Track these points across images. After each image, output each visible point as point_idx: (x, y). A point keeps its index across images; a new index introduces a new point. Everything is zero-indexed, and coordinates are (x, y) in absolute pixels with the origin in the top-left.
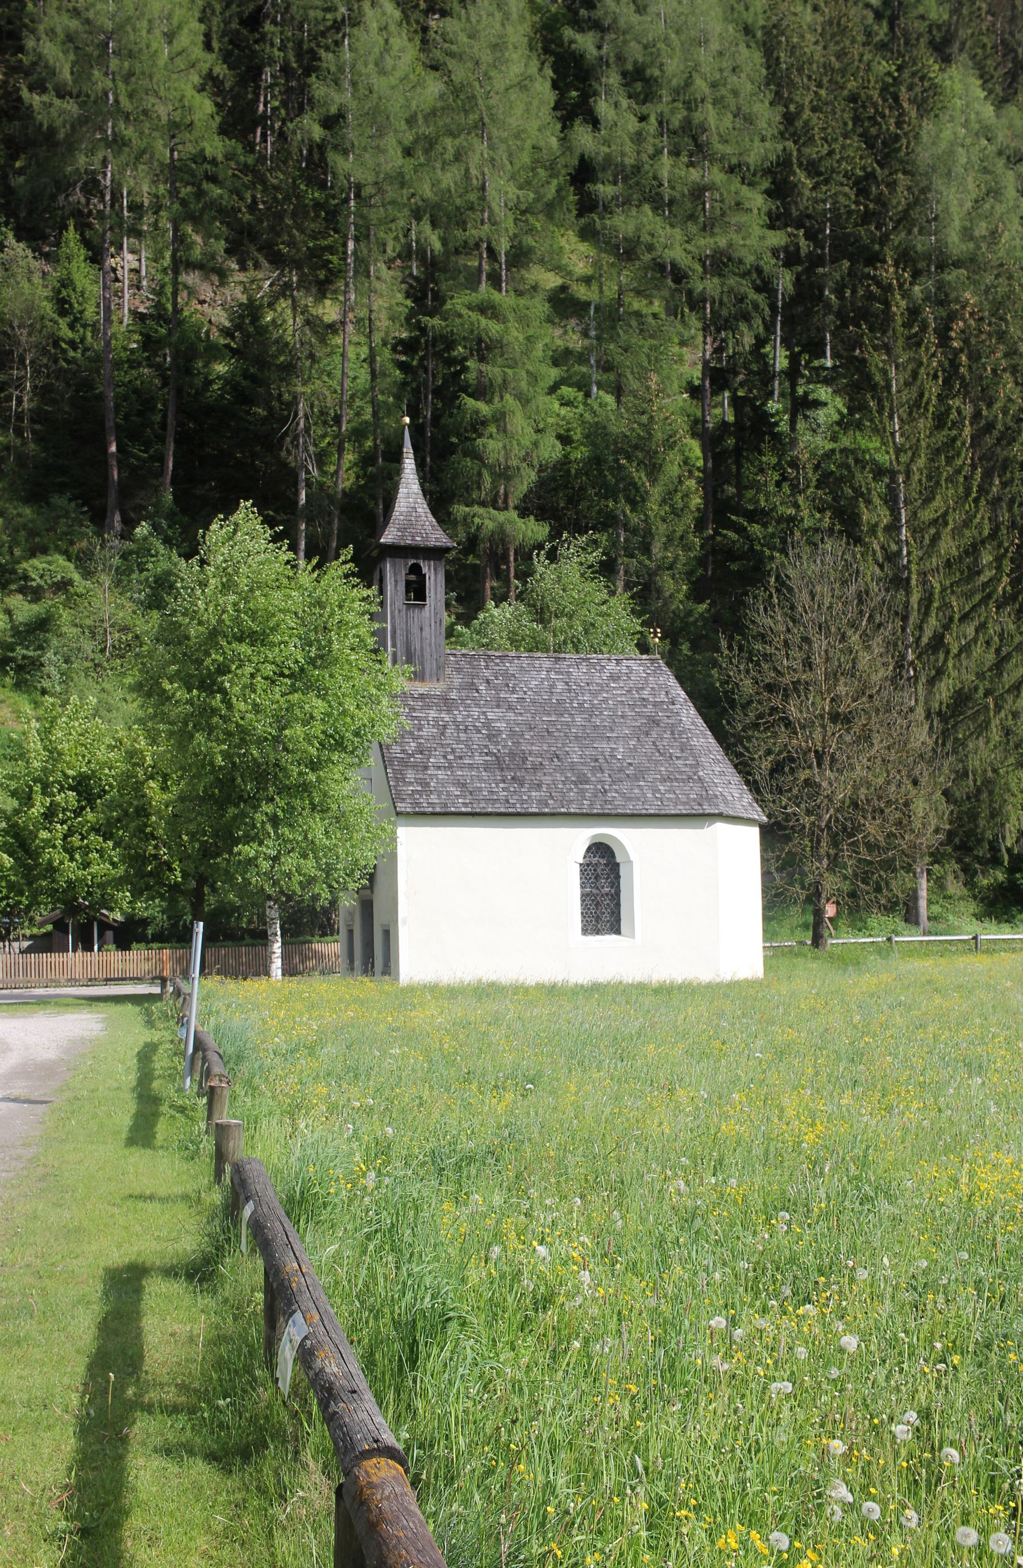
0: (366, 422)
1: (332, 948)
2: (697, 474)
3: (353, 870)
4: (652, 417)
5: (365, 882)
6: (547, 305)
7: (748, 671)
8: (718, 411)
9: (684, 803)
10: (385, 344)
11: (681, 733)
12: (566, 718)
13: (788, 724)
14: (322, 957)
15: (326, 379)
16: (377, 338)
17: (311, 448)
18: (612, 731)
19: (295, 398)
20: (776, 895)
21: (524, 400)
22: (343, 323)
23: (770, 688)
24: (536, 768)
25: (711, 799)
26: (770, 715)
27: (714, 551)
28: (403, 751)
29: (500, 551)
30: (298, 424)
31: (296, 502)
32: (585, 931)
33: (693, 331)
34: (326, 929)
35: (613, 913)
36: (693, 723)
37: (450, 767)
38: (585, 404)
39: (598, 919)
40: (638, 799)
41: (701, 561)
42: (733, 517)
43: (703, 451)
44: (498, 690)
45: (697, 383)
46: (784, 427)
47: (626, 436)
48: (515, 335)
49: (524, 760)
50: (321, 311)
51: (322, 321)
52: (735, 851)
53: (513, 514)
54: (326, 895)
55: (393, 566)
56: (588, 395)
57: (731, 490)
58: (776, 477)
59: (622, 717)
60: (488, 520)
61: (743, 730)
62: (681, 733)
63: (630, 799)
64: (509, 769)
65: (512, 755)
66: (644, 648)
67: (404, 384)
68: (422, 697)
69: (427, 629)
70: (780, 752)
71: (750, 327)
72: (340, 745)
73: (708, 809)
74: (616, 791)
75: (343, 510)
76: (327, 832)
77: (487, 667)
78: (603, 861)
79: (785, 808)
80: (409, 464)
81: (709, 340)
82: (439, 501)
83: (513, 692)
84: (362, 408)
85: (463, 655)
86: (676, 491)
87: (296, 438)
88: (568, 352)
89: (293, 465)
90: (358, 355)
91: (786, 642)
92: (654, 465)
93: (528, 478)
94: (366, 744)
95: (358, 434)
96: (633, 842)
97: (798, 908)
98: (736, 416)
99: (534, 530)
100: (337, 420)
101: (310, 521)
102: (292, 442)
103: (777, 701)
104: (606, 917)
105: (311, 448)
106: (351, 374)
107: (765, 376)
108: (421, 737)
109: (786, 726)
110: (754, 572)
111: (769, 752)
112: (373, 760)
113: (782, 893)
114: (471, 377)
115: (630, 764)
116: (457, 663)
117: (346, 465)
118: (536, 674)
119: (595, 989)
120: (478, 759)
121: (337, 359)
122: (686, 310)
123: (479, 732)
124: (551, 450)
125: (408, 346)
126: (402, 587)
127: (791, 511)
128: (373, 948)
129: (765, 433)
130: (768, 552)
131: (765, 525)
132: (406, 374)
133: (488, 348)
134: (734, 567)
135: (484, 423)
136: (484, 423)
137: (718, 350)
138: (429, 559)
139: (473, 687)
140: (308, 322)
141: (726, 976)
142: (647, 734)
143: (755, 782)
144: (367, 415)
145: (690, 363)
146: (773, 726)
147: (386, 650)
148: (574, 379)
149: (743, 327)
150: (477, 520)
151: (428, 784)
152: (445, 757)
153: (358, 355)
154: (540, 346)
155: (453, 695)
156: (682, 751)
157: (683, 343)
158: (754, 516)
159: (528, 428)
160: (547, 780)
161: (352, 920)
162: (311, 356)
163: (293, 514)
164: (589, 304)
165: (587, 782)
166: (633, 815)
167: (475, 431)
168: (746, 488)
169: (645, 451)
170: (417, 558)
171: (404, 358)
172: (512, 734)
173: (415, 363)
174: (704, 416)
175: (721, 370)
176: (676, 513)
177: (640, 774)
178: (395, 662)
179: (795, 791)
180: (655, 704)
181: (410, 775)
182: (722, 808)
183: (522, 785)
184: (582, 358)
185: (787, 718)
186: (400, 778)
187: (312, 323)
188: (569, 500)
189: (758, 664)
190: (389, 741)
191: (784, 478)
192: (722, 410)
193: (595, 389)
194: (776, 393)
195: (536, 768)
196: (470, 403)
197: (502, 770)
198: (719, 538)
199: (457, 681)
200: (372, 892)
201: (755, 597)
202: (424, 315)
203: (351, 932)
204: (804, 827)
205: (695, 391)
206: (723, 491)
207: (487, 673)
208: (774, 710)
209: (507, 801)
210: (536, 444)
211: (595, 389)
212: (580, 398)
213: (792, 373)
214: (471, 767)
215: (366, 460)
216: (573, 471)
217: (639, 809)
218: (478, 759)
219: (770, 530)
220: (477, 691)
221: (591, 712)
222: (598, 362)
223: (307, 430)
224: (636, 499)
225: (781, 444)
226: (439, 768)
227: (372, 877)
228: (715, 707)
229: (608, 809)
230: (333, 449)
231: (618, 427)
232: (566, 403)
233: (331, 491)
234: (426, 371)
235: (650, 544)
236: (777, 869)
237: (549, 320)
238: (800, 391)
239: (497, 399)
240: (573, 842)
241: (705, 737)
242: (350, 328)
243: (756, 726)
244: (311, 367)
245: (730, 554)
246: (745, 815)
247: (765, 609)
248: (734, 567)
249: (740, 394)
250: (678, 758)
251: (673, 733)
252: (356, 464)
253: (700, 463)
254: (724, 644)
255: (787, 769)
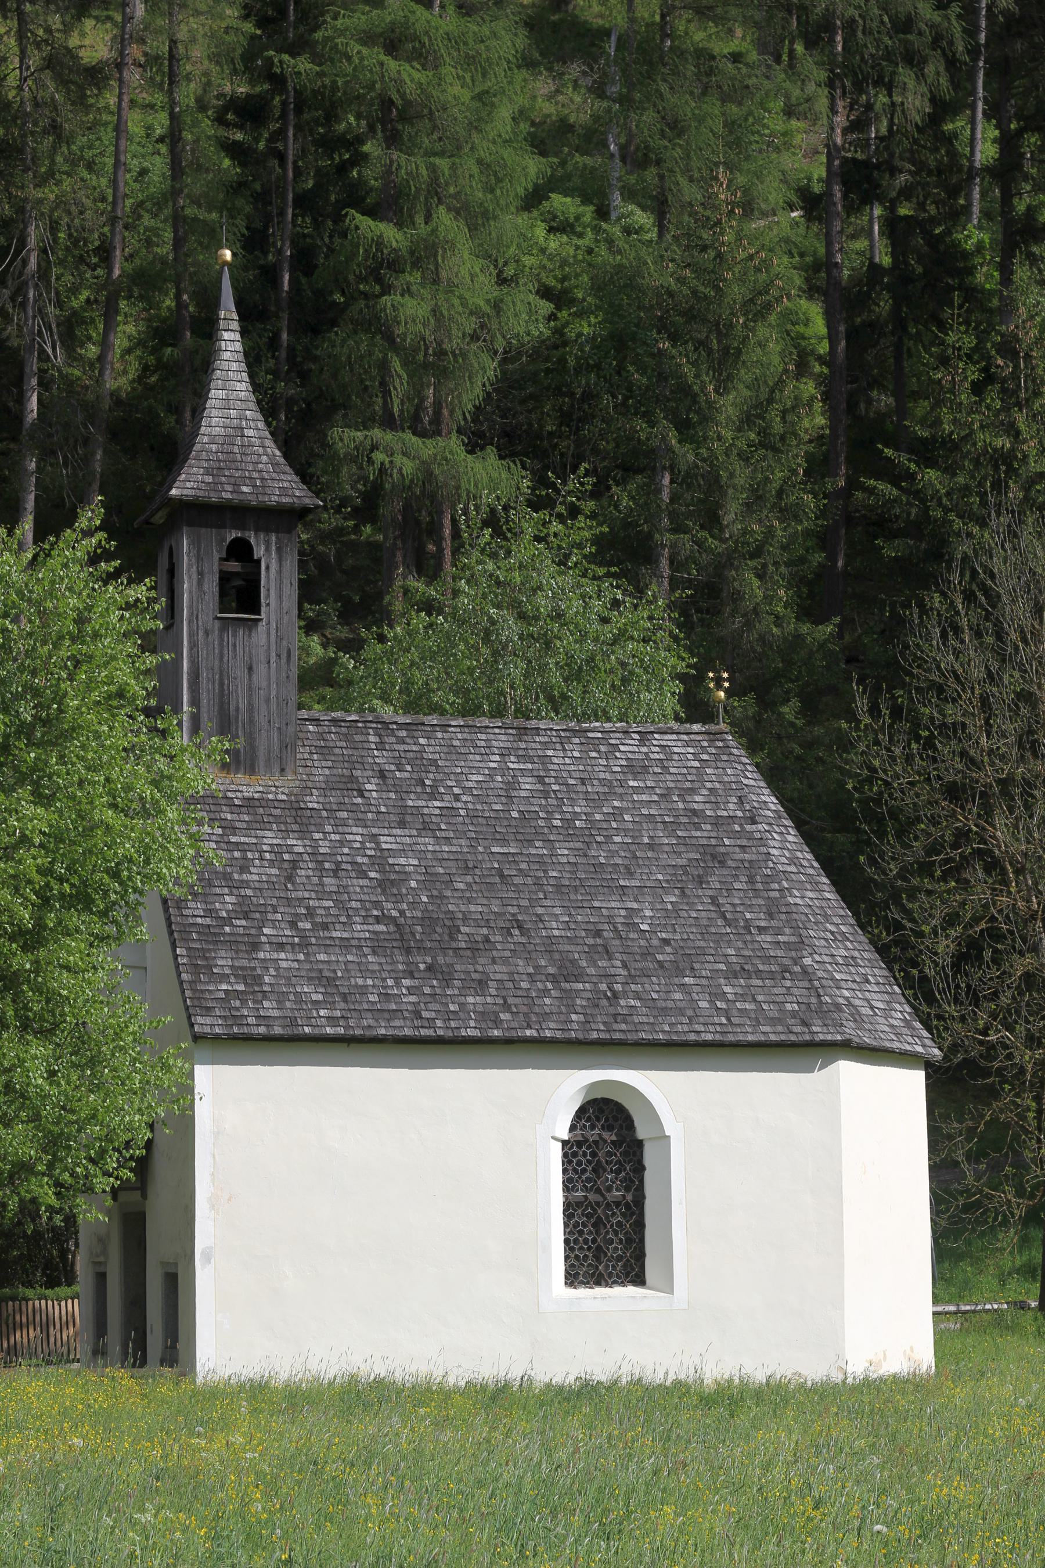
0: (163, 261)
1: (67, 1308)
2: (817, 368)
3: (103, 1152)
4: (719, 255)
5: (127, 1174)
6: (522, 32)
7: (909, 759)
8: (861, 244)
9: (773, 1021)
10: (202, 105)
11: (768, 879)
12: (539, 849)
13: (993, 865)
14: (46, 1326)
15: (85, 174)
16: (187, 94)
17: (51, 310)
18: (630, 874)
19: (21, 210)
20: (967, 1208)
21: (475, 218)
22: (120, 66)
23: (954, 792)
24: (478, 948)
25: (828, 1013)
26: (955, 846)
27: (849, 520)
28: (210, 913)
29: (424, 517)
30: (25, 262)
31: (19, 418)
32: (572, 1279)
33: (811, 87)
34: (58, 1274)
35: (629, 1241)
36: (793, 861)
37: (304, 945)
38: (597, 230)
39: (599, 1253)
40: (681, 1011)
41: (824, 540)
42: (888, 452)
43: (829, 326)
44: (402, 792)
45: (817, 188)
46: (986, 276)
47: (671, 294)
48: (455, 91)
49: (453, 931)
50: (73, 41)
51: (76, 58)
52: (876, 1120)
53: (455, 444)
54: (49, 1197)
55: (195, 543)
56: (603, 213)
57: (884, 400)
58: (973, 374)
59: (651, 846)
60: (402, 454)
61: (901, 876)
62: (768, 879)
63: (665, 1011)
64: (422, 949)
65: (428, 921)
66: (695, 708)
67: (237, 188)
68: (249, 803)
69: (261, 669)
70: (976, 920)
71: (920, 77)
72: (81, 899)
73: (821, 1032)
74: (637, 996)
75: (114, 434)
76: (52, 1074)
77: (381, 746)
78: (610, 1137)
79: (985, 1032)
80: (230, 342)
81: (840, 104)
82: (298, 419)
83: (433, 796)
84: (155, 231)
85: (334, 721)
86: (770, 401)
87: (20, 290)
88: (564, 127)
89: (15, 342)
90: (149, 128)
91: (984, 700)
92: (726, 351)
93: (484, 371)
94: (132, 897)
95: (145, 282)
96: (672, 1098)
97: (1009, 1237)
98: (893, 255)
99: (490, 478)
100: (105, 253)
101: (47, 454)
102: (13, 299)
103: (968, 819)
104: (615, 1249)
105: (51, 310)
106: (135, 164)
107: (952, 176)
108: (246, 884)
109: (988, 870)
110: (928, 557)
111: (951, 920)
112: (148, 929)
113: (978, 1204)
114: (371, 175)
115: (666, 942)
116: (321, 736)
117: (119, 342)
118: (480, 762)
119: (585, 1395)
120: (361, 930)
121: (108, 136)
122: (799, 48)
123: (363, 875)
124: (527, 319)
125: (248, 112)
126: (212, 585)
127: (1003, 442)
128: (145, 1313)
129: (952, 289)
130: (958, 524)
131: (950, 471)
132: (243, 165)
133: (405, 117)
134: (890, 551)
135: (395, 265)
136: (395, 265)
137: (857, 126)
138: (268, 531)
139: (352, 785)
140: (50, 63)
141: (857, 1367)
142: (700, 881)
143: (924, 979)
144: (165, 250)
145: (802, 147)
146: (959, 869)
147: (177, 709)
148: (576, 181)
149: (905, 75)
150: (379, 456)
151: (258, 980)
152: (293, 925)
153: (149, 128)
154: (505, 113)
155: (313, 801)
156: (771, 915)
157: (789, 112)
158: (927, 452)
159: (482, 274)
160: (499, 971)
161: (105, 1252)
162: (55, 128)
163: (15, 439)
164: (607, 33)
165: (578, 978)
166: (669, 1045)
167: (379, 280)
168: (916, 396)
169: (702, 323)
170: (243, 528)
171: (239, 136)
172: (430, 879)
173: (262, 145)
174: (829, 253)
175: (866, 164)
176: (768, 443)
177: (685, 962)
178: (195, 729)
179: (1005, 1000)
180: (717, 822)
181: (223, 962)
182: (850, 1031)
183: (447, 982)
184: (592, 139)
185: (990, 853)
186: (202, 966)
187: (61, 64)
188: (579, 415)
189: (929, 743)
190: (178, 892)
191: (989, 377)
192: (866, 243)
193: (617, 198)
194: (976, 209)
195: (478, 948)
196: (365, 225)
197: (408, 951)
198: (859, 494)
199: (321, 772)
200: (144, 1196)
201: (924, 610)
202: (280, 50)
203: (101, 1278)
204: (1022, 1071)
205: (813, 204)
206: (869, 402)
207: (381, 758)
208: (962, 836)
209: (417, 1014)
210: (497, 306)
211: (617, 198)
212: (587, 219)
213: (1006, 171)
214: (345, 945)
215: (161, 334)
216: (571, 362)
217: (683, 1031)
218: (361, 930)
219: (961, 480)
220: (361, 793)
221: (588, 837)
222: (623, 148)
223: (43, 273)
224: (691, 418)
225: (986, 311)
226: (281, 947)
227: (143, 1166)
228: (844, 832)
229: (620, 1030)
230: (96, 313)
231: (661, 276)
232: (559, 226)
233: (90, 396)
234: (282, 158)
235: (719, 506)
236: (968, 1157)
237: (527, 63)
238: (1020, 206)
239: (419, 219)
240: (550, 1097)
241: (816, 887)
242: (134, 76)
243: (925, 869)
244: (54, 149)
245: (880, 524)
246: (896, 1045)
247: (944, 635)
248: (890, 551)
249: (903, 211)
250: (761, 930)
251: (751, 880)
252: (141, 343)
253: (824, 348)
254: (862, 704)
255: (987, 954)
